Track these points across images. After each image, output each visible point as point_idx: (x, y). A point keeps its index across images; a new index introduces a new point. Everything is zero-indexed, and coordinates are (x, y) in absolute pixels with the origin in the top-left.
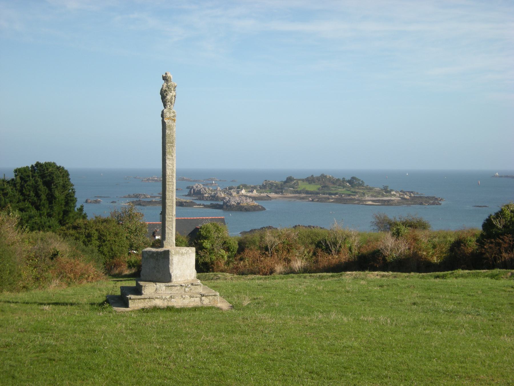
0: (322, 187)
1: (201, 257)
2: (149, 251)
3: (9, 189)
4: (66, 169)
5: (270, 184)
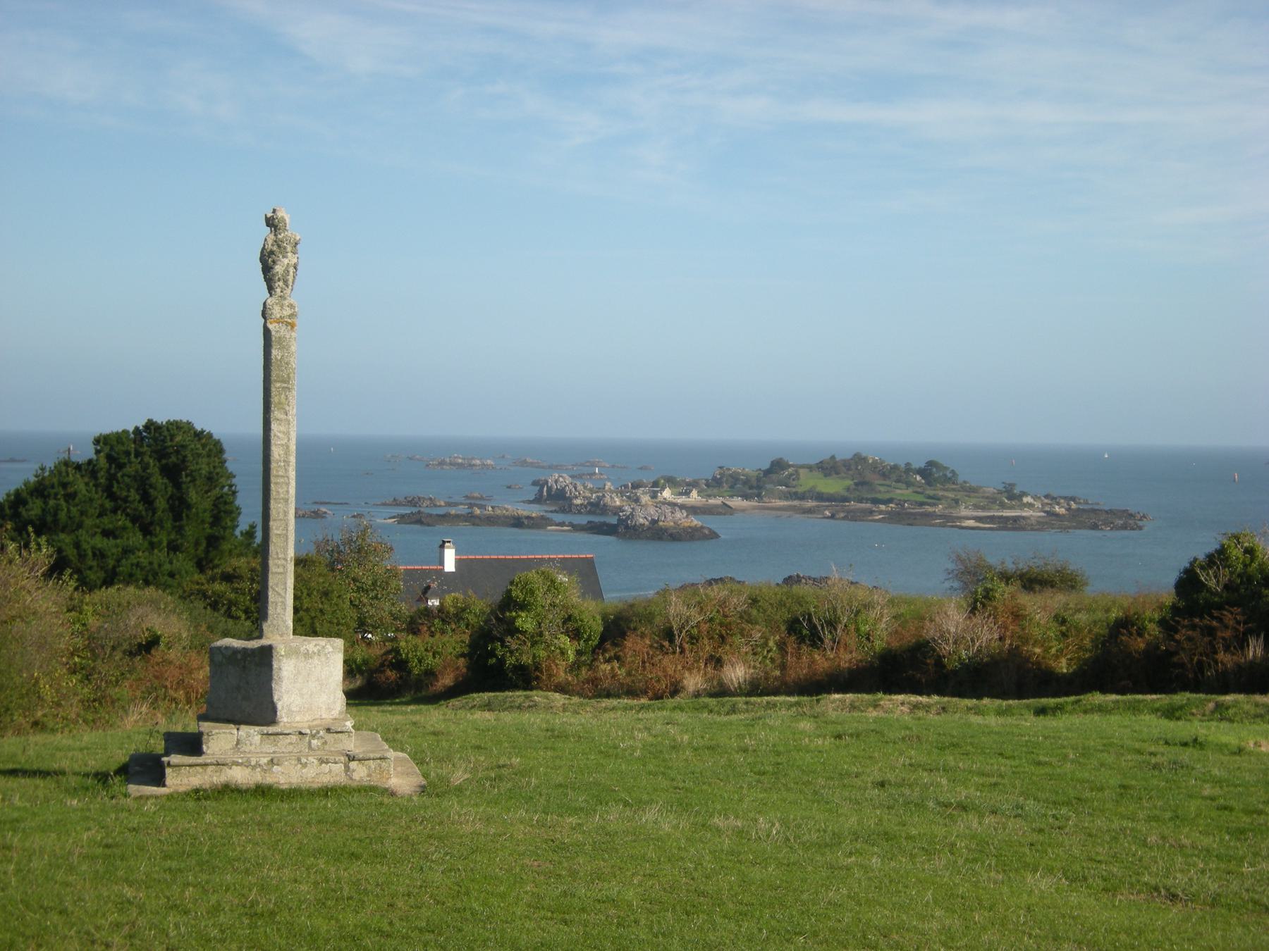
0: (856, 484)
1: (511, 652)
2: (227, 648)
3: (81, 485)
4: (216, 437)
5: (731, 476)
